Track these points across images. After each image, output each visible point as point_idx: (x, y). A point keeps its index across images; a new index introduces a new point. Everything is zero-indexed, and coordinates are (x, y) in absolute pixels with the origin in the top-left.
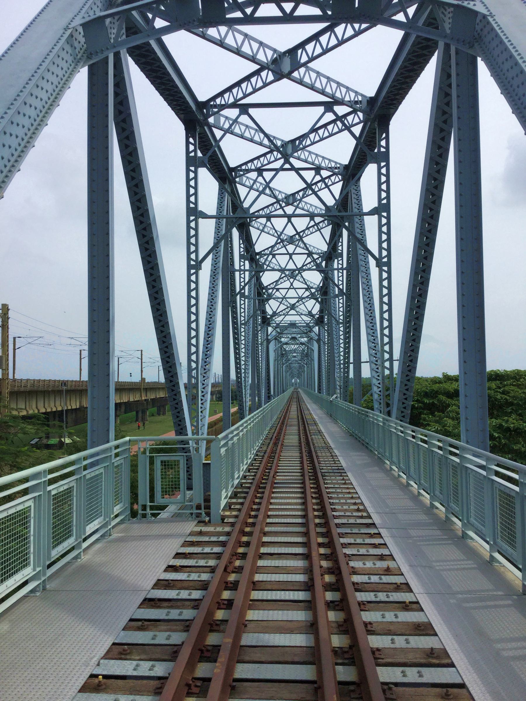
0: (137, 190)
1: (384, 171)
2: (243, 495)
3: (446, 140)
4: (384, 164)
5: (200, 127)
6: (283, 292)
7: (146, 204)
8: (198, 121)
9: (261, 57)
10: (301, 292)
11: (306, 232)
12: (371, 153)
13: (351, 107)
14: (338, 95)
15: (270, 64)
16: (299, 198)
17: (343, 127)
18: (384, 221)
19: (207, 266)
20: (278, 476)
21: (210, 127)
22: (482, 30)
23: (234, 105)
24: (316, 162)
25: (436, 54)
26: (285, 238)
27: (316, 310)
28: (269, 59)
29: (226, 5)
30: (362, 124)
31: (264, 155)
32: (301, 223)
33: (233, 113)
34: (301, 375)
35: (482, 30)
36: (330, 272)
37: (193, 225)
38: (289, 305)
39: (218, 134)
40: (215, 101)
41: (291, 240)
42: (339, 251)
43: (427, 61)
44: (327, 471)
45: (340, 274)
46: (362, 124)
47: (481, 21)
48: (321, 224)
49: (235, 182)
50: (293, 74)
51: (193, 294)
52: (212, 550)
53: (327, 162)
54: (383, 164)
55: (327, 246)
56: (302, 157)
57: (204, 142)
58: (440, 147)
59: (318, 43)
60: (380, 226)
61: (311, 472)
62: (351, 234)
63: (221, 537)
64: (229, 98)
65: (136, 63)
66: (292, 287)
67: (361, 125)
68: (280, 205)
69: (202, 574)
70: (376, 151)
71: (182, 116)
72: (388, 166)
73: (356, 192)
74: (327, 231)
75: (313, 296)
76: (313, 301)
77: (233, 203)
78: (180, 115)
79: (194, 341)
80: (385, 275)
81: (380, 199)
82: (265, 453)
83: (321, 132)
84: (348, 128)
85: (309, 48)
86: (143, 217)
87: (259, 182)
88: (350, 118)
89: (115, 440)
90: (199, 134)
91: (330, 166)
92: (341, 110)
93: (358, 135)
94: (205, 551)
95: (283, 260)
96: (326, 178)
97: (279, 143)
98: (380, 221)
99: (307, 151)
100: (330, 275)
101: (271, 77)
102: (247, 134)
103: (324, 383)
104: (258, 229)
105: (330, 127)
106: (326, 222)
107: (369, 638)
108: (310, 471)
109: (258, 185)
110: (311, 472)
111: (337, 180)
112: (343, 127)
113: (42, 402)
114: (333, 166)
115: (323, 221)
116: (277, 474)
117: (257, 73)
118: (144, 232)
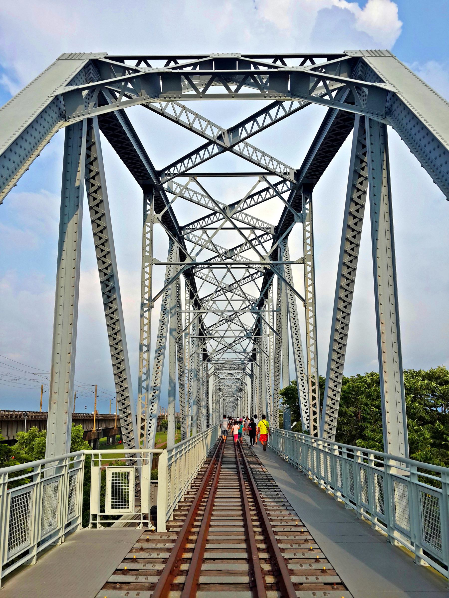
1: (308, 228)
2: (186, 508)
5: (156, 191)
6: (222, 333)
8: (153, 185)
9: (208, 132)
10: (237, 333)
11: (242, 281)
12: (298, 214)
13: (281, 177)
14: (271, 166)
15: (215, 139)
16: (236, 252)
17: (275, 194)
19: (158, 304)
20: (218, 492)
21: (164, 191)
22: (391, 106)
23: (183, 174)
24: (252, 223)
25: (352, 132)
26: (224, 286)
27: (250, 349)
28: (215, 135)
29: (182, 86)
30: (290, 191)
31: (209, 216)
32: (239, 274)
33: (183, 180)
34: (236, 408)
35: (391, 106)
37: (147, 270)
38: (226, 345)
39: (170, 197)
40: (169, 170)
41: (230, 289)
42: (270, 298)
43: (344, 139)
44: (262, 487)
45: (271, 317)
46: (290, 191)
47: (390, 99)
48: (255, 275)
49: (184, 238)
50: (234, 148)
51: (146, 328)
52: (158, 555)
53: (260, 223)
55: (259, 293)
56: (240, 218)
57: (159, 204)
59: (255, 122)
61: (248, 489)
62: (281, 279)
63: (167, 544)
64: (181, 168)
65: (105, 135)
66: (229, 329)
69: (149, 577)
70: (302, 212)
71: (141, 182)
73: (284, 248)
74: (260, 281)
75: (248, 336)
76: (248, 340)
77: (181, 252)
78: (140, 181)
80: (311, 314)
82: (205, 472)
83: (256, 198)
84: (279, 194)
85: (248, 126)
87: (203, 239)
88: (280, 187)
90: (155, 197)
91: (262, 226)
92: (273, 180)
93: (286, 200)
94: (152, 556)
95: (222, 306)
96: (259, 237)
97: (221, 206)
99: (244, 214)
100: (262, 316)
101: (216, 150)
102: (195, 198)
104: (201, 278)
105: (263, 194)
106: (259, 273)
108: (247, 487)
109: (203, 241)
110: (248, 489)
111: (268, 238)
112: (275, 194)
113: (6, 430)
114: (265, 227)
115: (256, 273)
116: (218, 490)
117: (205, 147)
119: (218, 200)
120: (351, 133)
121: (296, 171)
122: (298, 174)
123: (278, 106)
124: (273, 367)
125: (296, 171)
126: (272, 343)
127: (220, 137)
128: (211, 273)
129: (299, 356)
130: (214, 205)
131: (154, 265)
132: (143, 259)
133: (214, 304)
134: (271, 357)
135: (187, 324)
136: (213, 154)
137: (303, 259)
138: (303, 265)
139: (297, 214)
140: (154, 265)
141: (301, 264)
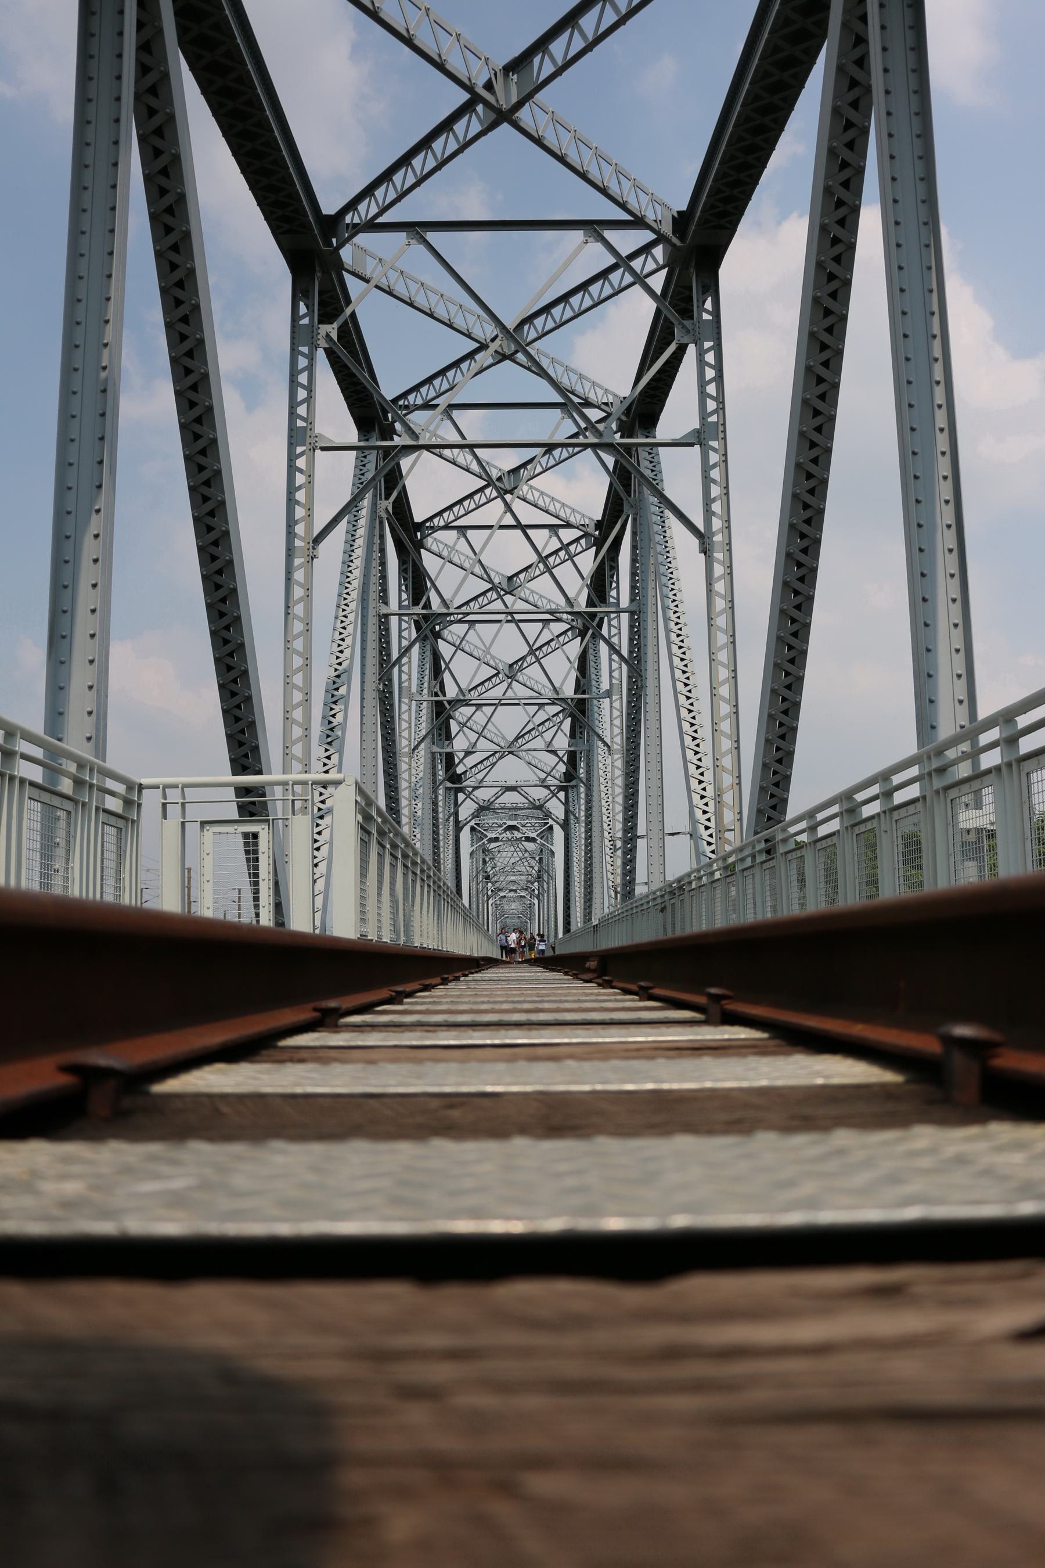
0: (153, 102)
1: (710, 357)
3: (856, 145)
4: (710, 420)
7: (181, 180)
18: (714, 457)
36: (595, 702)
54: (708, 345)
58: (844, 165)
60: (706, 468)
65: (192, 68)
67: (664, 272)
68: (498, 593)
72: (718, 349)
79: (297, 714)
81: (704, 414)
84: (640, 280)
86: (178, 252)
89: (96, 806)
93: (659, 292)
98: (705, 458)
103: (578, 909)
107: (725, 750)
118: (179, 293)
119: (489, 566)
120: (818, 61)
121: (676, 215)
122: (681, 221)
123: (644, 255)
124: (621, 808)
125: (676, 215)
126: (618, 713)
127: (499, 479)
128: (463, 540)
129: (679, 635)
130: (483, 572)
131: (318, 452)
132: (290, 437)
133: (471, 632)
134: (616, 747)
135: (405, 660)
136: (480, 504)
137: (697, 433)
138: (697, 447)
139: (680, 323)
140: (318, 452)
141: (692, 445)
